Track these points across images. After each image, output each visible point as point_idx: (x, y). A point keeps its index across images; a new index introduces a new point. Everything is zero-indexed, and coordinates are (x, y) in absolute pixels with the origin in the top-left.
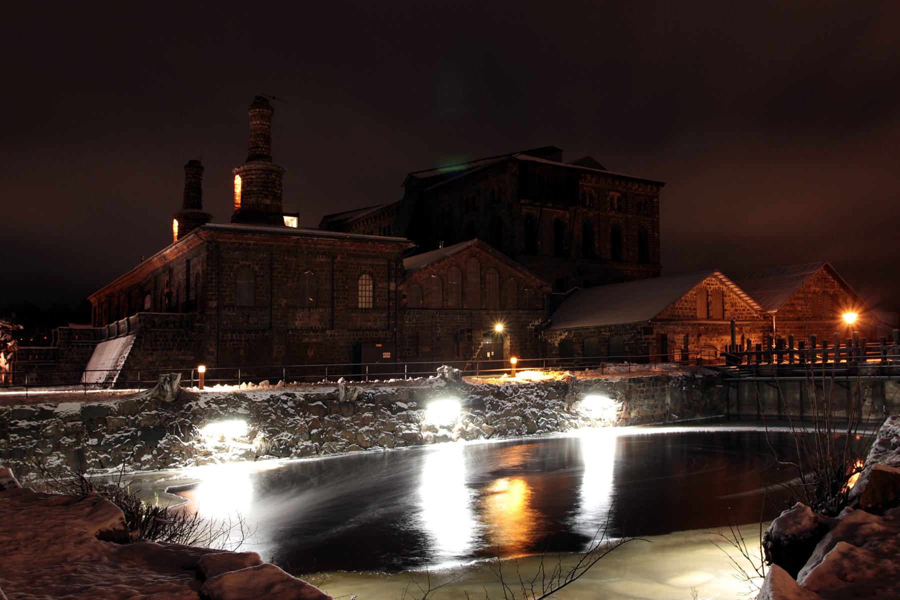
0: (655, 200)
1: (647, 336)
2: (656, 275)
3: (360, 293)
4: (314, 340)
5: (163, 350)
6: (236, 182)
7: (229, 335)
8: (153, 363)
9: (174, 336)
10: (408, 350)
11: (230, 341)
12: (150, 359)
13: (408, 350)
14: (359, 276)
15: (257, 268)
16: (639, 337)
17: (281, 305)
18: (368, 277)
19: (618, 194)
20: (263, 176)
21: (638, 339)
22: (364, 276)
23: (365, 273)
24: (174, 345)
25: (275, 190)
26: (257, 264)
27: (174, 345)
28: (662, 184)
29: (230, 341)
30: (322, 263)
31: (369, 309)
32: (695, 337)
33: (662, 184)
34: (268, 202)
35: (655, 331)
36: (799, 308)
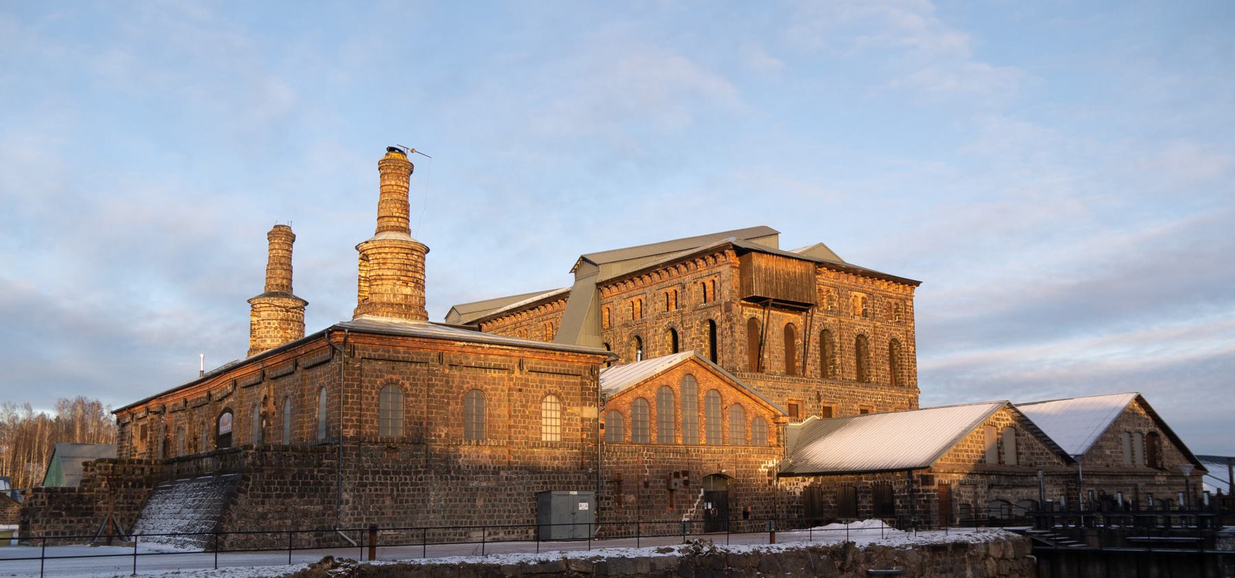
0: (909, 303)
1: (926, 488)
2: (912, 405)
3: (544, 421)
4: (484, 484)
5: (278, 496)
6: (1121, 397)
7: (370, 476)
8: (263, 516)
9: (294, 477)
10: (607, 499)
11: (371, 484)
12: (260, 509)
13: (607, 499)
14: (542, 398)
15: (407, 385)
16: (915, 487)
17: (440, 436)
18: (554, 399)
19: (864, 295)
20: (401, 256)
21: (913, 491)
22: (549, 398)
23: (550, 393)
24: (294, 490)
25: (417, 275)
26: (408, 379)
27: (294, 490)
28: (917, 283)
29: (371, 484)
30: (494, 379)
31: (556, 443)
32: (986, 488)
33: (917, 283)
34: (408, 291)
35: (936, 480)
36: (1108, 452)
